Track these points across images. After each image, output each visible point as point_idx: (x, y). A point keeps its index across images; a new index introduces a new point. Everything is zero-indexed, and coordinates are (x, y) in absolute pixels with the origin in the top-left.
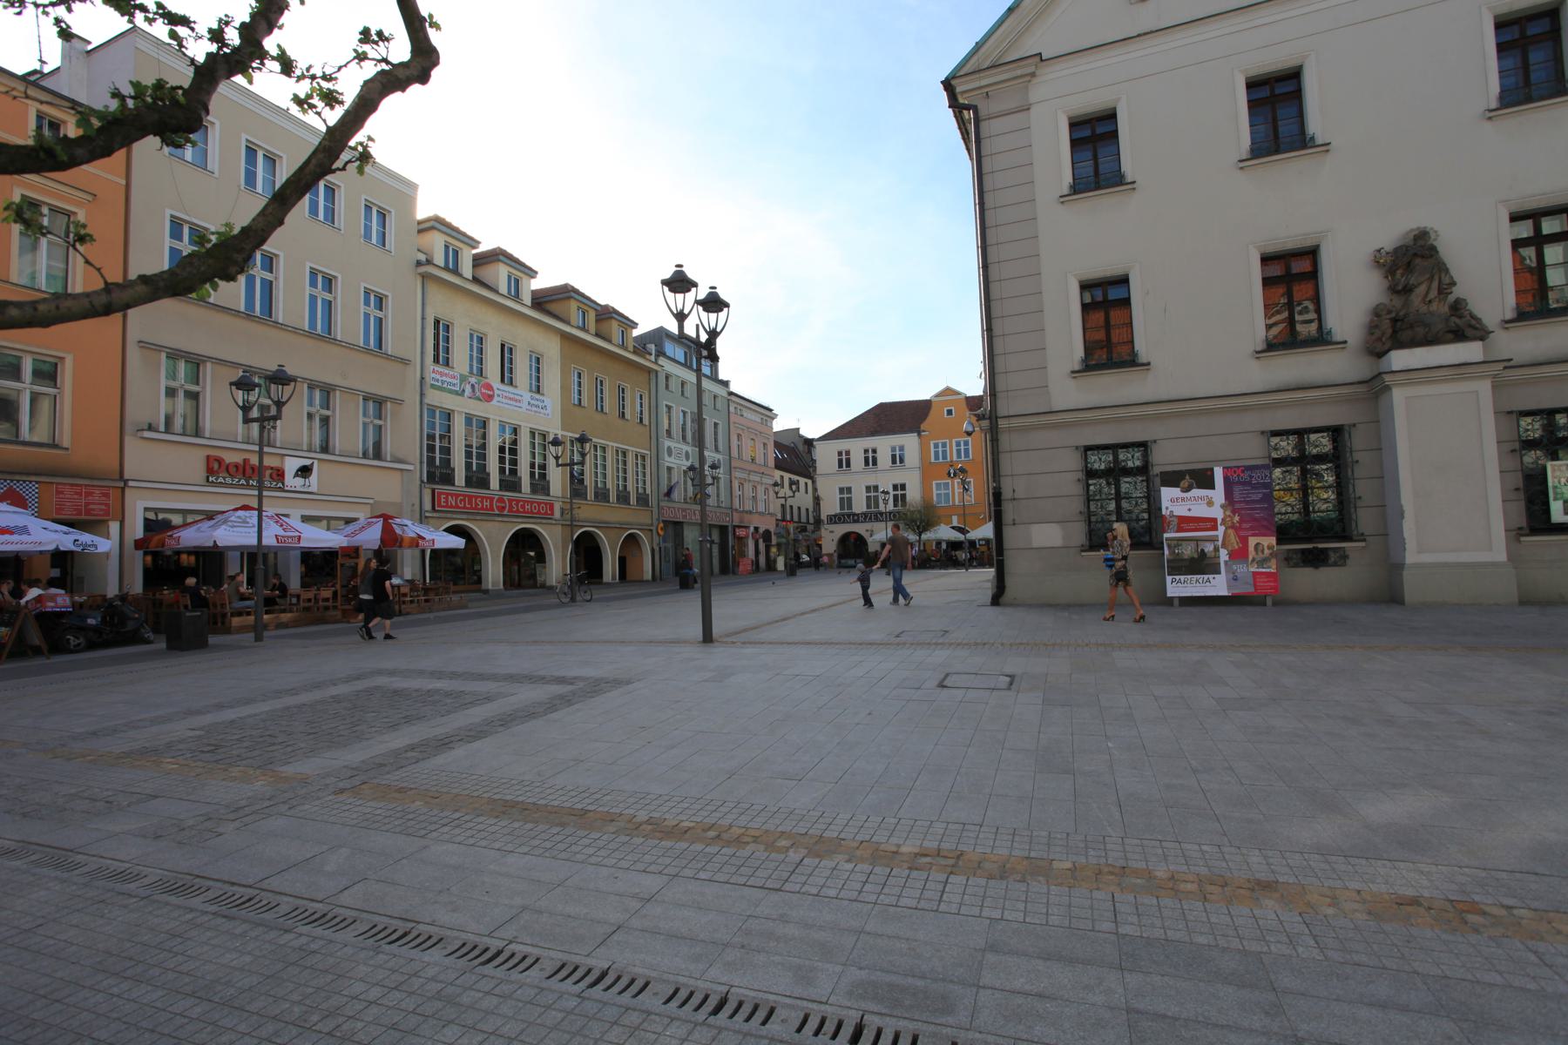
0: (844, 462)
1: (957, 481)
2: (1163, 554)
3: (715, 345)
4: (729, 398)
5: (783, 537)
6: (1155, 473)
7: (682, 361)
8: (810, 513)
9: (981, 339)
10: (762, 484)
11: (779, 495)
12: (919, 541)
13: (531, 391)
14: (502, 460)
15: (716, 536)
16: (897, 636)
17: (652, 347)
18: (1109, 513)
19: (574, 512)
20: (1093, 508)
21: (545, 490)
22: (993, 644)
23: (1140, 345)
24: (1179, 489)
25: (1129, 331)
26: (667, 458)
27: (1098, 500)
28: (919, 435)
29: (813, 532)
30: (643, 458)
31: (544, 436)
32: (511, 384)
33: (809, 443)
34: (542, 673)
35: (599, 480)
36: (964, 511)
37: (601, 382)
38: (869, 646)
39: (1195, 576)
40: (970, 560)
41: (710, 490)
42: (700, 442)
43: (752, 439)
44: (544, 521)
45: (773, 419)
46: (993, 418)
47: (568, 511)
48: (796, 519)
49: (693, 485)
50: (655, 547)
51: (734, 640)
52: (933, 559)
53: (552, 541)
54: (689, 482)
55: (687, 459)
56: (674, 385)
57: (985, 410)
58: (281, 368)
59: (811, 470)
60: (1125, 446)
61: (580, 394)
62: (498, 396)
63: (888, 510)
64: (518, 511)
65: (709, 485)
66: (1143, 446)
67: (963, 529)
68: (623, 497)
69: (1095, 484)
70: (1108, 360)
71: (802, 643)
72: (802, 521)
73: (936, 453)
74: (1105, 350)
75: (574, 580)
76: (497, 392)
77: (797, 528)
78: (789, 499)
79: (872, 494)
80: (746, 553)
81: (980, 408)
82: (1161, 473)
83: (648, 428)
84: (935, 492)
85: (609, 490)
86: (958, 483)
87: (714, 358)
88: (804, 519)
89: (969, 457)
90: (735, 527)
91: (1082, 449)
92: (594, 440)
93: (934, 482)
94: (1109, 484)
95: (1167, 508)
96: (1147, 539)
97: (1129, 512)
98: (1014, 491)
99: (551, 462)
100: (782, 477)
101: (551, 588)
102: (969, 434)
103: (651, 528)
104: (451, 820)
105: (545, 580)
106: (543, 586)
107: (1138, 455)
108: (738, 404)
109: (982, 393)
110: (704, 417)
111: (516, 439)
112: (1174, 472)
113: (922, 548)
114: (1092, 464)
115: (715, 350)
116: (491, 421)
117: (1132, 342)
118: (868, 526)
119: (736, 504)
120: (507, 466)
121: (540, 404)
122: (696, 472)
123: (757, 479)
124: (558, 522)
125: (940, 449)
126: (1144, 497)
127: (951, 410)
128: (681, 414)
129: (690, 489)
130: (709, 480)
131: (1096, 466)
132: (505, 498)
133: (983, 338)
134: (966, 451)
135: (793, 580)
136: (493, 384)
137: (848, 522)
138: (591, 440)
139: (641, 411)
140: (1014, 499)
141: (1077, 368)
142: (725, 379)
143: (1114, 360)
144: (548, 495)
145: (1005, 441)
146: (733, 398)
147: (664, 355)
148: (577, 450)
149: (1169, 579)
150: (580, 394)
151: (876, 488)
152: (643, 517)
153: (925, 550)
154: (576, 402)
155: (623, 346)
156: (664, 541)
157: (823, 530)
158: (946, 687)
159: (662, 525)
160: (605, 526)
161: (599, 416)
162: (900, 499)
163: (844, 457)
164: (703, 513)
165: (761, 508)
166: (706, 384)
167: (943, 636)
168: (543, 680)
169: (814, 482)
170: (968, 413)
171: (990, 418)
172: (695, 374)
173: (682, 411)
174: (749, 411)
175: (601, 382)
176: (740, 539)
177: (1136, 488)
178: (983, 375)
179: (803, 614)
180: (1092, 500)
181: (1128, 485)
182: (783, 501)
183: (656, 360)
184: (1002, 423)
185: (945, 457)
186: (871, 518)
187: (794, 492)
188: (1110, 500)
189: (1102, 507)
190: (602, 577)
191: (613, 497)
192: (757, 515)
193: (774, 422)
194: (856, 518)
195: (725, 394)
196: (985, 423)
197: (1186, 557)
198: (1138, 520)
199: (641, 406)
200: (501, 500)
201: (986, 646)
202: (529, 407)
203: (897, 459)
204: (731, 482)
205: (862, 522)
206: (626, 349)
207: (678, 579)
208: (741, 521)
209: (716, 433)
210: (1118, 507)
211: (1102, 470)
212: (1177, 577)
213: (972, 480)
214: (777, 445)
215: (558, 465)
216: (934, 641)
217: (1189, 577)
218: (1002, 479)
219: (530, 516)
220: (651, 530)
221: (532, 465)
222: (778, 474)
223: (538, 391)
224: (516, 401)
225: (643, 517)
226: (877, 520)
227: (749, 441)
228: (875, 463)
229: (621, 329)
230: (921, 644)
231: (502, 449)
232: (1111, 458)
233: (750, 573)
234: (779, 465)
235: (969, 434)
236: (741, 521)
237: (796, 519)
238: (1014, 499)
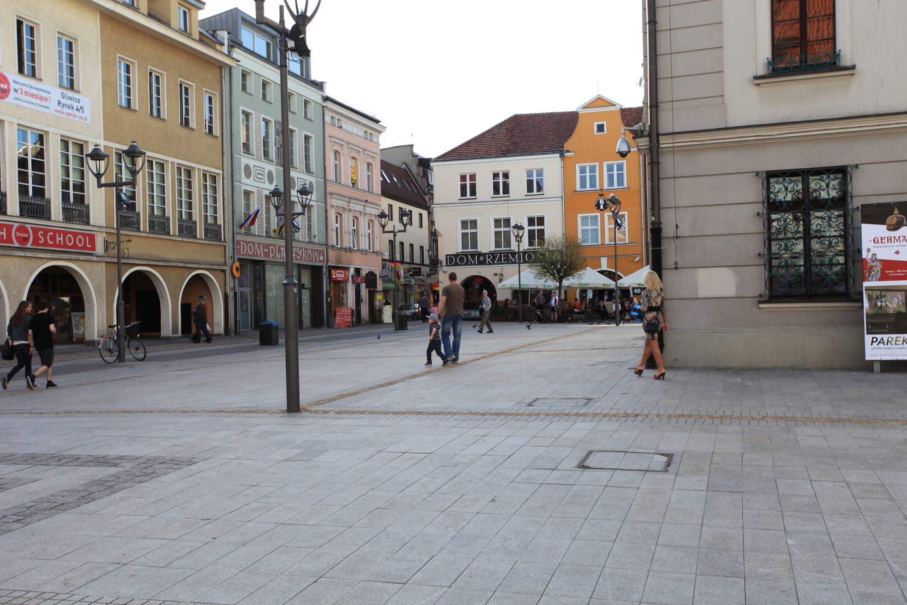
0: (468, 188)
1: (608, 214)
2: (862, 307)
3: (305, 33)
4: (324, 104)
5: (390, 281)
6: (855, 207)
7: (264, 55)
8: (426, 254)
9: (642, 34)
10: (365, 214)
11: (386, 229)
12: (560, 288)
13: (61, 86)
14: (23, 176)
15: (306, 279)
16: (530, 405)
17: (224, 35)
18: (795, 256)
19: (122, 247)
20: (775, 248)
21: (84, 217)
22: (647, 416)
23: (843, 43)
24: (884, 227)
25: (831, 26)
26: (244, 179)
27: (782, 239)
28: (562, 156)
29: (429, 275)
30: (214, 178)
31: (81, 146)
32: (33, 75)
33: (425, 164)
34: (75, 452)
35: (155, 206)
36: (615, 252)
37: (157, 78)
38: (495, 417)
39: (902, 336)
40: (621, 312)
41: (299, 221)
42: (286, 161)
43: (353, 158)
44: (82, 257)
45: (380, 132)
46: (654, 134)
47: (115, 244)
48: (407, 258)
49: (278, 215)
50: (228, 291)
51: (328, 409)
52: (576, 310)
53: (92, 281)
54: (273, 210)
55: (271, 181)
56: (253, 85)
57: (644, 125)
58: (97, 147)
59: (427, 198)
60: (818, 172)
61: (129, 93)
62: (16, 91)
63: (521, 250)
64: (46, 243)
65: (299, 214)
66: (842, 172)
67: (614, 274)
68: (187, 229)
69: (778, 220)
70: (801, 62)
71: (413, 413)
72: (415, 261)
73: (583, 179)
74: (799, 49)
75: (123, 333)
76: (13, 86)
77: (409, 271)
78: (399, 234)
79: (502, 229)
80: (344, 301)
81: (637, 123)
82: (862, 205)
83: (220, 140)
84: (580, 228)
85: (168, 219)
86: (609, 216)
87: (303, 51)
88: (417, 259)
89: (623, 185)
90: (330, 268)
91: (764, 175)
92: (148, 153)
93: (579, 215)
94: (796, 219)
95: (869, 250)
96: (841, 288)
97: (821, 255)
98: (677, 227)
99: (91, 181)
100: (391, 206)
101: (93, 343)
102: (623, 155)
103: (224, 268)
104: (40, 597)
105: (84, 334)
106: (81, 341)
107: (834, 183)
108: (335, 112)
109: (641, 105)
110: (290, 127)
111: (42, 150)
112: (879, 205)
113: (563, 297)
114: (776, 194)
115: (304, 40)
116: (51, 135)
117: (834, 39)
118: (497, 268)
119: (333, 240)
120: (30, 185)
121: (75, 105)
122: (280, 196)
123: (359, 208)
124: (99, 259)
125: (588, 174)
126: (840, 236)
127: (603, 125)
128: (263, 123)
129: (274, 219)
130: (298, 209)
131: (781, 197)
132: (28, 226)
133: (645, 33)
134: (620, 177)
135: (403, 334)
136: (7, 75)
137: (472, 264)
138: (144, 154)
139: (211, 118)
140: (677, 237)
141: (761, 72)
142: (319, 80)
143: (809, 62)
144: (88, 224)
145: (668, 164)
146: (329, 104)
147: (240, 45)
148: (126, 166)
149: (868, 338)
150: (129, 93)
151: (507, 222)
152: (213, 255)
153: (566, 299)
154: (124, 104)
155: (185, 32)
156: (241, 286)
157: (441, 274)
158: (588, 467)
159: (237, 264)
160: (164, 265)
161: (155, 124)
162: (537, 236)
163: (468, 182)
164: (289, 249)
165: (364, 244)
166: (293, 85)
167: (586, 404)
168: (77, 461)
169: (430, 213)
170: (623, 128)
171: (649, 135)
172: (279, 72)
173: (264, 119)
174: (347, 121)
175: (157, 78)
176: (337, 283)
177: (830, 226)
178: (643, 81)
179: (414, 376)
180: (774, 240)
181: (819, 221)
182: (391, 236)
183: (229, 52)
184: (665, 142)
185: (593, 185)
186: (500, 259)
187: (405, 226)
188: (797, 239)
189: (786, 248)
190: (159, 330)
191: (174, 228)
192: (358, 254)
193: (382, 136)
194: (481, 259)
195: (320, 100)
196: (644, 142)
197: (891, 311)
198: (831, 265)
199: (211, 112)
200: (22, 229)
201: (639, 418)
202: (60, 108)
203: (534, 186)
204: (326, 211)
205: (490, 264)
206: (189, 36)
207: (258, 332)
208: (339, 260)
209: (307, 149)
210: (807, 248)
211: (788, 202)
212: (879, 337)
213: (626, 213)
214: (385, 166)
215: (100, 185)
216: (574, 411)
217: (894, 336)
218: (662, 211)
219: (63, 250)
220: (224, 271)
221: (65, 185)
222: (385, 202)
223: (72, 87)
224: (41, 98)
225: (213, 255)
226: (508, 261)
227: (350, 159)
228: (506, 190)
229: (182, 8)
230: (558, 415)
231: (22, 163)
232: (800, 187)
233: (349, 326)
234: (387, 191)
235: (623, 155)
236: (339, 261)
237: (407, 258)
238: (677, 237)
